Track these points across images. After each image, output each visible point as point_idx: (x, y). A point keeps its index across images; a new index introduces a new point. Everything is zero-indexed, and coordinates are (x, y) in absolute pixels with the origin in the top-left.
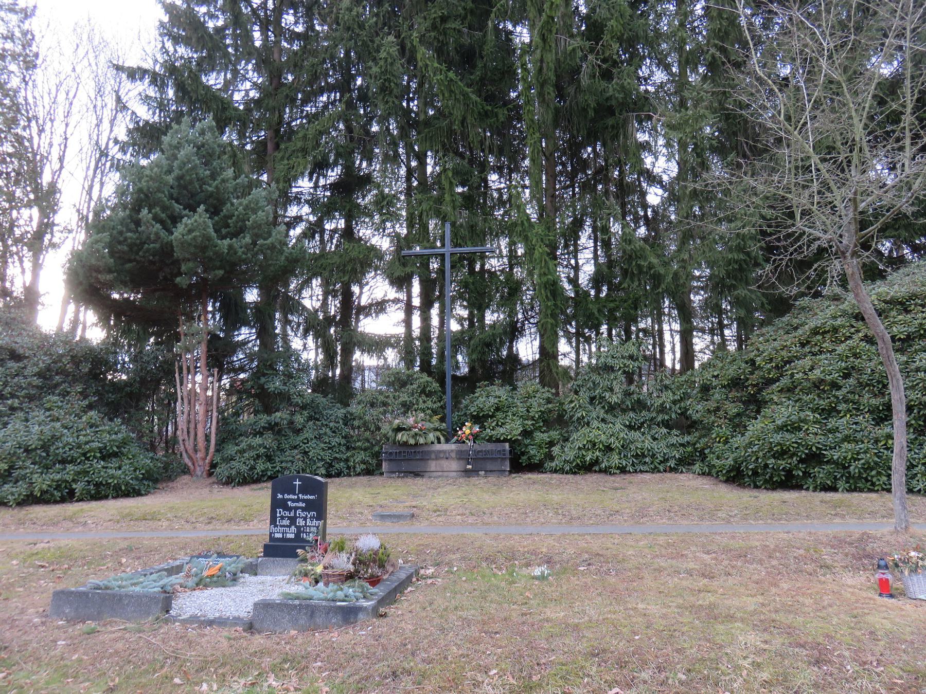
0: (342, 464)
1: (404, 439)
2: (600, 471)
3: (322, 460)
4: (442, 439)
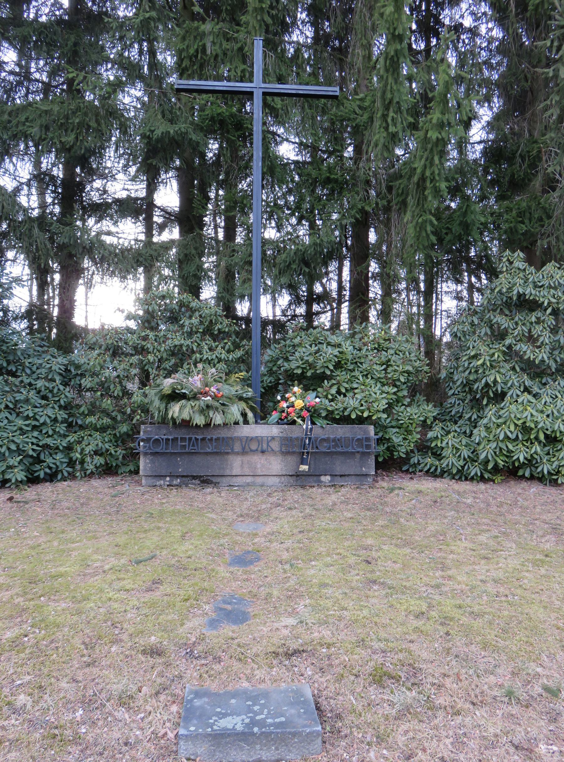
0: (59, 456)
1: (185, 416)
2: (541, 479)
3: (19, 451)
4: (250, 415)
